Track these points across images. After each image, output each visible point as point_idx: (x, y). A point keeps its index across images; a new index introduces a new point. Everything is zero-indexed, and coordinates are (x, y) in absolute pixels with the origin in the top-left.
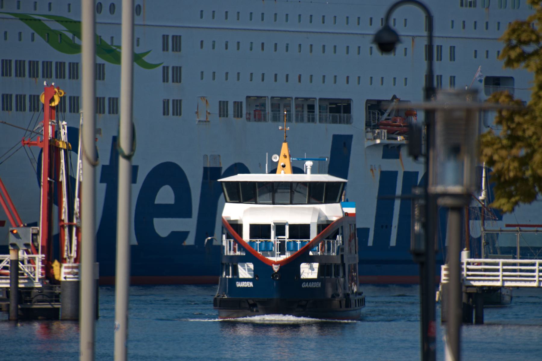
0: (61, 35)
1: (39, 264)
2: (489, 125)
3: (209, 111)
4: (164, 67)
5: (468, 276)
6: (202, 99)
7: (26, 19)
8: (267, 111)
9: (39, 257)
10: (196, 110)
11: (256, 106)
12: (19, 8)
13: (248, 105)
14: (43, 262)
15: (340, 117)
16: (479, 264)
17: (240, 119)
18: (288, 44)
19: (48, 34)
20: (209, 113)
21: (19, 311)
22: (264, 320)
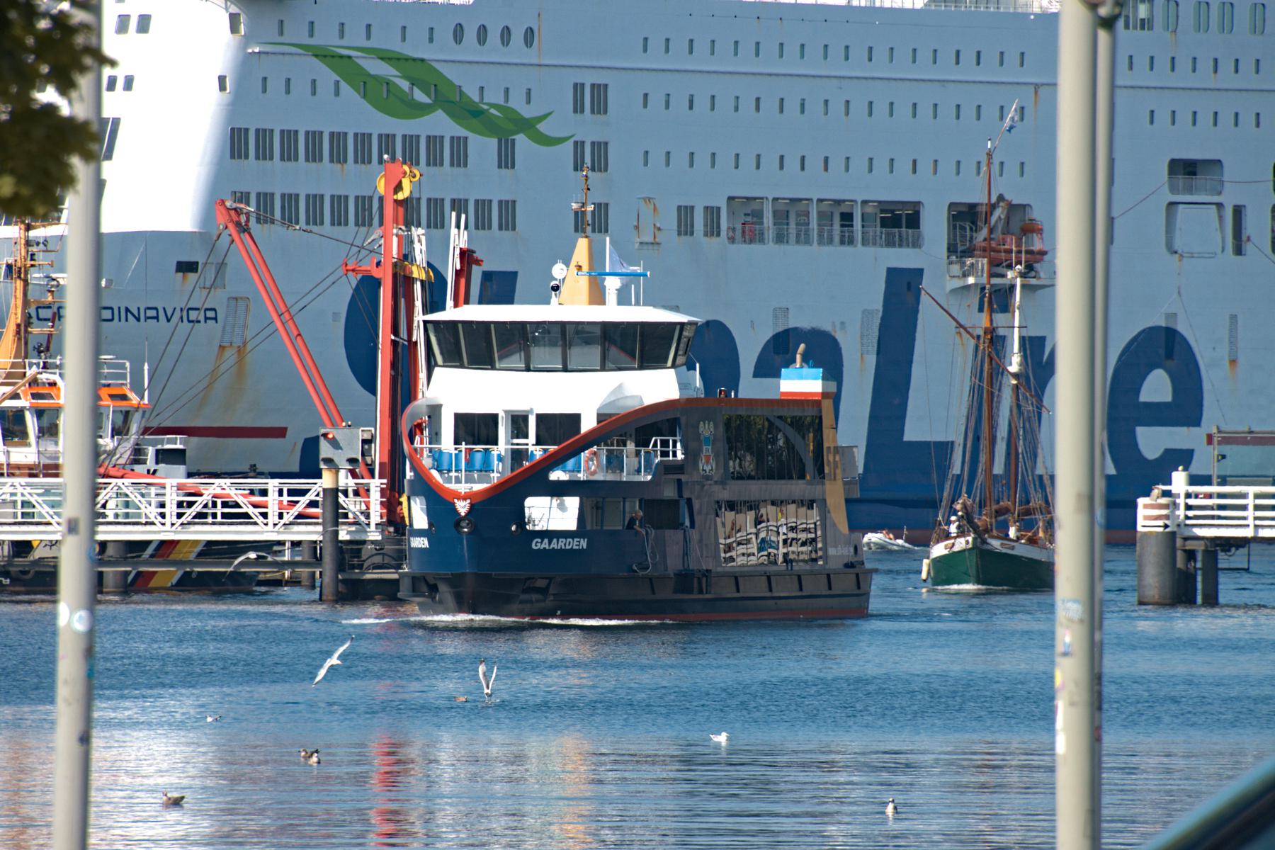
0: (388, 84)
1: (375, 498)
2: (1176, 248)
3: (658, 225)
4: (576, 143)
5: (1187, 518)
6: (646, 202)
7: (324, 55)
8: (766, 225)
9: (376, 484)
10: (636, 224)
11: (745, 215)
12: (311, 35)
13: (731, 213)
14: (383, 492)
15: (900, 236)
16: (1210, 496)
17: (715, 240)
18: (804, 100)
19: (365, 83)
20: (659, 229)
21: (340, 584)
22: (454, 616)
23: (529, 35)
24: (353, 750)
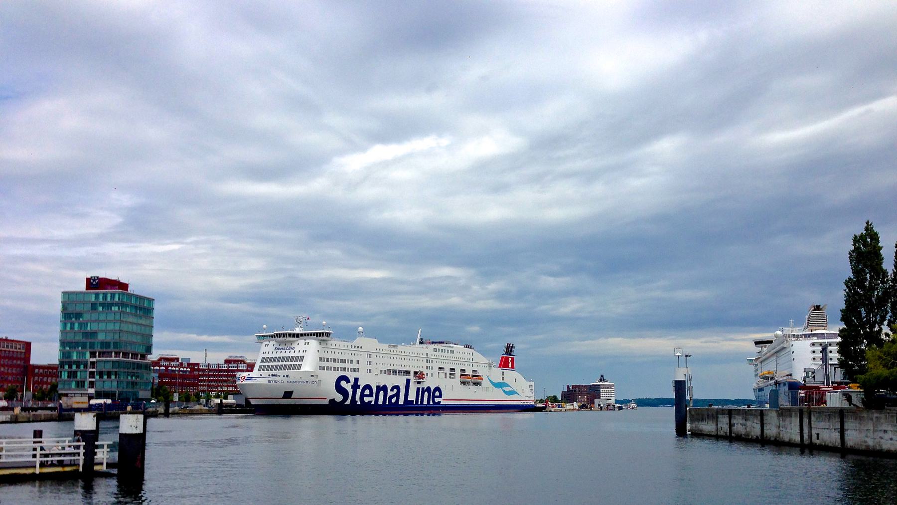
23: (361, 347)
24: (51, 439)
